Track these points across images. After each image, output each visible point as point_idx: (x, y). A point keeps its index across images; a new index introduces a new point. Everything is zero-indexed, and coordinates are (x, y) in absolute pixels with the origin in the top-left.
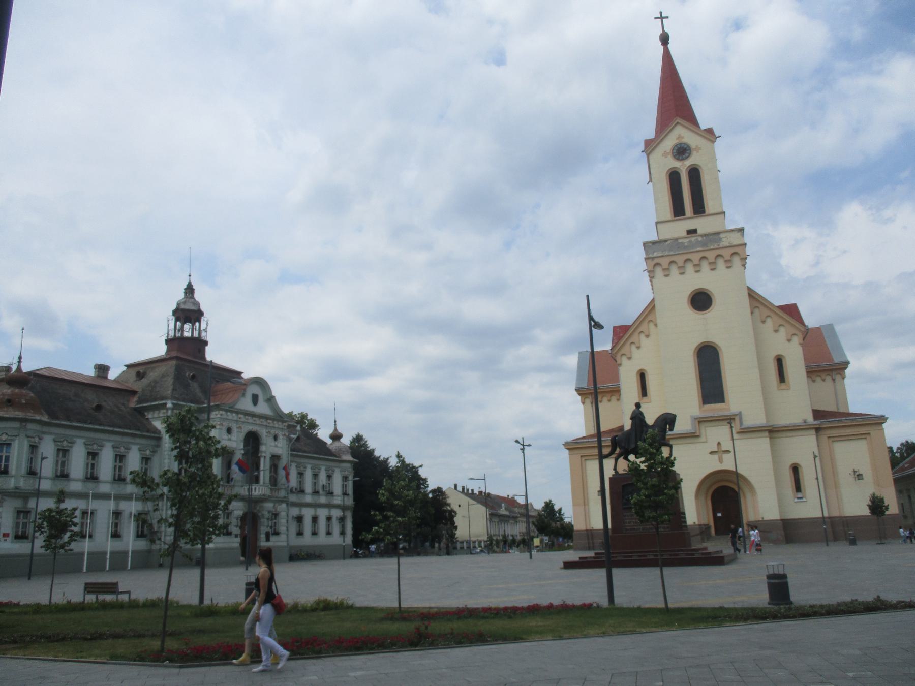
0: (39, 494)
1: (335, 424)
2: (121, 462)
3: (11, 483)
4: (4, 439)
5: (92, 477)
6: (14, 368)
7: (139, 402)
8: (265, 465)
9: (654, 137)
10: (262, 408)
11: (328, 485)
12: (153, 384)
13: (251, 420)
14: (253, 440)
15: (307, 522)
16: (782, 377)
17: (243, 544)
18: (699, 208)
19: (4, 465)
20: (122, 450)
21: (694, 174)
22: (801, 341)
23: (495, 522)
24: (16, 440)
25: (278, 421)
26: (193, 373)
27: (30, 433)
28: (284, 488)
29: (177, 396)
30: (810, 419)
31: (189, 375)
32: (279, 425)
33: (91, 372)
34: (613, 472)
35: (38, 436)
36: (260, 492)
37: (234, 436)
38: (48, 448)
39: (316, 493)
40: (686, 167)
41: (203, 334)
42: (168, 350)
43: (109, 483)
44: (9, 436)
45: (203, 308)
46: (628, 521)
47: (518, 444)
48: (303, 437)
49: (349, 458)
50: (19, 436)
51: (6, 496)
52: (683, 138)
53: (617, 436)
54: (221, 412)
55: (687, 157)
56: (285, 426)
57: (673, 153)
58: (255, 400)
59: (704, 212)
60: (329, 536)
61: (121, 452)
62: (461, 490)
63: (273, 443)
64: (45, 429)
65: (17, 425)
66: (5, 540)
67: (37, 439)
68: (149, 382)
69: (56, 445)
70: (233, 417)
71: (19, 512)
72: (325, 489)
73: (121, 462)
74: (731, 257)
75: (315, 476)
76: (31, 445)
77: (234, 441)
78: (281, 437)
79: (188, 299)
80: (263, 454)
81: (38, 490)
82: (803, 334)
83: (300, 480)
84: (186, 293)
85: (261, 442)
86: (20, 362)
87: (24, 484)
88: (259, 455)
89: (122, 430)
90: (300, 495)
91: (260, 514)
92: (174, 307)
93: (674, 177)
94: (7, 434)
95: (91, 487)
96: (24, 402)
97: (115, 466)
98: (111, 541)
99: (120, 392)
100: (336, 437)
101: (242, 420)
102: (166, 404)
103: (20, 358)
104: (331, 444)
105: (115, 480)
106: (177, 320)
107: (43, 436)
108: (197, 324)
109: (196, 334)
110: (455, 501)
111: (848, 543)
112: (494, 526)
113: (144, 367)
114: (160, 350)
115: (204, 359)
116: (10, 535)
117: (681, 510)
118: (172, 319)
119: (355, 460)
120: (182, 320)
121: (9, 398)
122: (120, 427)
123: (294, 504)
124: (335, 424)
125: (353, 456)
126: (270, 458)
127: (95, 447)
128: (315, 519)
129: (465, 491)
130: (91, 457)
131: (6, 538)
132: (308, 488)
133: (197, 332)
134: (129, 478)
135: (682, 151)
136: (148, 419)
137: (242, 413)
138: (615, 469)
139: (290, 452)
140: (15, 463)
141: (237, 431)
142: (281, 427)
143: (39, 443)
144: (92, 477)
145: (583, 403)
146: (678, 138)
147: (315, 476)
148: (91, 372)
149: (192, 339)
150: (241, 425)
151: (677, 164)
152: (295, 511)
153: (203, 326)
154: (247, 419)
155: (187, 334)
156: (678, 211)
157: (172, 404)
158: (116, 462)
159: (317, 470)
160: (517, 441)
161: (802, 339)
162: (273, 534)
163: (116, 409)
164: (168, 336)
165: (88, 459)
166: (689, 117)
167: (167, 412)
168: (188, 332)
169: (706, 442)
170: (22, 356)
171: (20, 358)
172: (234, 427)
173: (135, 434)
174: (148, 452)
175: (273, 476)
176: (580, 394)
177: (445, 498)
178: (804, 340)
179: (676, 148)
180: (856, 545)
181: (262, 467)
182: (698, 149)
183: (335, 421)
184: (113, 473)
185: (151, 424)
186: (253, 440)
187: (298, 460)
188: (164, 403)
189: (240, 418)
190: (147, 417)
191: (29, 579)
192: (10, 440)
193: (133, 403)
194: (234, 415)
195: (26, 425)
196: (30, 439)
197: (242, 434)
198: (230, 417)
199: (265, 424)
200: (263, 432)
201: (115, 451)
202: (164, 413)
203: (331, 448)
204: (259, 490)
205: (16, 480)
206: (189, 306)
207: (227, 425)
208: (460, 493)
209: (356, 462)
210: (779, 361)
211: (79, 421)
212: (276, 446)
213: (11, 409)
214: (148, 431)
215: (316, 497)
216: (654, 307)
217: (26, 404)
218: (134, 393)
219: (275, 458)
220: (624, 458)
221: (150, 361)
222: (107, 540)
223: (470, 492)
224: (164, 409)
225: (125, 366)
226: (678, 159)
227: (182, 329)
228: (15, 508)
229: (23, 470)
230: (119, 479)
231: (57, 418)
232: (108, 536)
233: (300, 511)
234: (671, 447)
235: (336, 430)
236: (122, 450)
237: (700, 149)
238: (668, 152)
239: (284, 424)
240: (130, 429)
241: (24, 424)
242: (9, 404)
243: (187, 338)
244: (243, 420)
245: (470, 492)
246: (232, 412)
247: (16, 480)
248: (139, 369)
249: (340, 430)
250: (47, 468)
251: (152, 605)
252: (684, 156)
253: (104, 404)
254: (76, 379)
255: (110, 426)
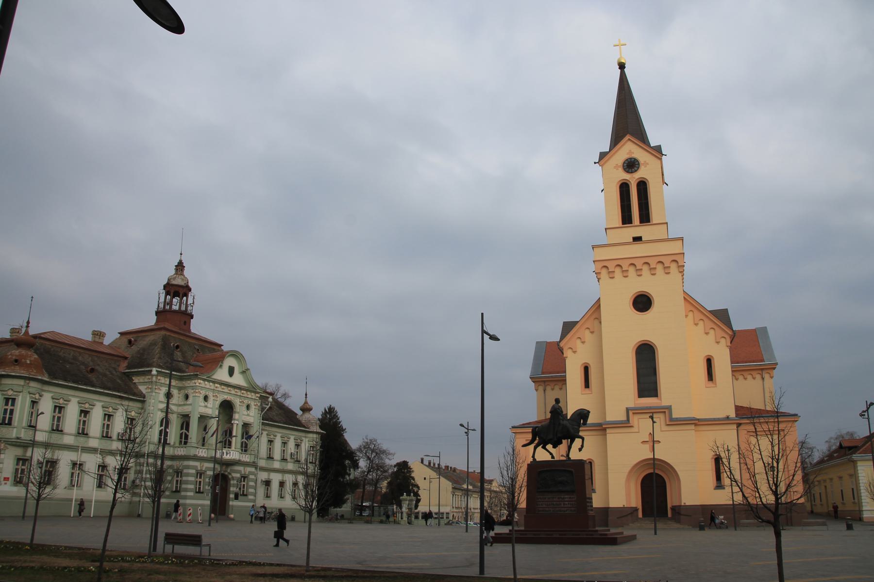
0: (33, 444)
1: (306, 397)
2: (109, 420)
3: (13, 433)
4: (10, 394)
5: (83, 433)
6: (24, 330)
7: (128, 367)
8: (237, 431)
9: (652, 146)
10: (238, 379)
11: (296, 453)
12: (141, 352)
13: (226, 390)
14: (227, 407)
15: (275, 486)
16: (710, 376)
17: (214, 501)
18: (645, 218)
19: (6, 415)
20: (111, 410)
21: (642, 186)
22: (729, 344)
23: (458, 495)
24: (19, 395)
25: (251, 391)
26: (178, 344)
27: (31, 390)
28: (254, 453)
29: (161, 365)
30: (732, 414)
31: (174, 345)
32: (248, 395)
33: (89, 338)
34: (531, 459)
35: (39, 393)
36: (234, 457)
37: (210, 403)
38: (46, 405)
39: (284, 460)
40: (634, 180)
41: (189, 308)
42: (158, 321)
43: (98, 439)
44: (14, 391)
45: (190, 285)
46: (540, 503)
47: (463, 428)
48: (275, 407)
49: (317, 429)
50: (22, 392)
51: (9, 445)
52: (633, 153)
53: (537, 427)
54: (199, 381)
55: (636, 171)
56: (257, 397)
57: (623, 166)
58: (231, 371)
59: (649, 221)
60: (268, 499)
61: (109, 412)
62: (427, 464)
63: (245, 412)
64: (46, 388)
65: (22, 382)
66: (5, 484)
67: (37, 396)
68: (139, 349)
69: (54, 402)
70: (210, 386)
71: (19, 460)
72: (293, 457)
73: (109, 420)
74: (628, 268)
75: (284, 444)
76: (32, 401)
77: (210, 408)
78: (253, 407)
79: (178, 276)
80: (236, 422)
81: (34, 441)
82: (730, 337)
83: (269, 446)
84: (176, 270)
85: (234, 410)
86: (27, 326)
87: (25, 435)
88: (232, 422)
89: (111, 392)
90: (270, 462)
91: (230, 476)
92: (165, 282)
93: (624, 188)
94: (12, 390)
95: (82, 440)
96: (28, 362)
97: (104, 424)
98: (96, 491)
99: (112, 356)
100: (306, 409)
101: (217, 389)
102: (151, 371)
103: (28, 323)
104: (302, 415)
105: (103, 437)
106: (167, 293)
107: (43, 393)
108: (185, 298)
109: (183, 308)
110: (420, 474)
111: (698, 529)
112: (457, 499)
113: (135, 336)
114: (150, 320)
115: (189, 330)
116: (10, 479)
117: (588, 496)
118: (163, 293)
119: (322, 431)
120: (172, 294)
121: (17, 358)
122: (109, 389)
123: (263, 469)
124: (306, 397)
125: (321, 427)
126: (242, 425)
127: (87, 406)
128: (282, 484)
129: (432, 465)
130: (83, 414)
131: (6, 482)
132: (277, 455)
133: (184, 306)
134: (115, 437)
135: (631, 165)
136: (135, 383)
137: (218, 383)
138: (533, 456)
139: (261, 421)
140: (17, 416)
141: (213, 400)
142: (254, 397)
143: (39, 399)
144: (83, 433)
145: (537, 390)
146: (628, 154)
147: (284, 444)
148: (89, 338)
149: (179, 312)
150: (216, 394)
151: (626, 176)
152: (263, 476)
153: (190, 301)
154: (223, 389)
155: (175, 307)
156: (627, 219)
157: (157, 371)
158: (104, 420)
159: (286, 439)
160: (462, 425)
161: (729, 342)
162: (241, 495)
163: (108, 373)
164: (158, 309)
165: (80, 416)
166: (641, 136)
167: (152, 378)
168: (176, 305)
169: (639, 432)
170: (30, 321)
171: (28, 323)
172: (210, 394)
173: (123, 397)
174: (133, 414)
175: (245, 442)
176: (533, 382)
177: (410, 472)
178: (731, 342)
179: (627, 162)
180: (853, 530)
181: (234, 434)
182: (646, 164)
183: (306, 395)
184: (102, 430)
185: (138, 388)
186: (227, 407)
187: (267, 428)
188: (149, 370)
189: (216, 387)
190: (134, 382)
191: (217, 522)
192: (15, 395)
193: (123, 367)
194: (211, 384)
195: (28, 383)
196: (31, 395)
197: (217, 402)
198: (250, 396)
199: (239, 394)
200: (237, 402)
201: (104, 411)
202: (149, 379)
203: (300, 419)
204: (233, 454)
205: (18, 430)
206: (179, 281)
207: (204, 393)
208: (425, 467)
209: (323, 433)
210: (709, 362)
211: (74, 382)
212: (248, 415)
213: (17, 368)
214: (134, 394)
215: (284, 464)
216: (599, 306)
217: (30, 364)
218: (126, 358)
219: (246, 426)
220: (542, 447)
221: (146, 329)
222: (93, 490)
223: (437, 466)
224: (150, 375)
225: (119, 333)
226: (628, 172)
227: (171, 304)
228: (16, 456)
229: (25, 424)
230: (106, 436)
231: (56, 378)
232: (94, 487)
233: (269, 475)
234: (583, 439)
235: (306, 403)
236: (111, 410)
237: (648, 164)
238: (619, 165)
239: (257, 395)
240: (119, 392)
241: (28, 382)
242: (16, 364)
243: (175, 311)
244: (220, 389)
245: (437, 466)
246: (209, 381)
247: (18, 430)
248: (131, 337)
249: (311, 403)
250: (44, 422)
251: (82, 553)
252: (633, 170)
253: (97, 368)
254: (75, 343)
255: (101, 388)
